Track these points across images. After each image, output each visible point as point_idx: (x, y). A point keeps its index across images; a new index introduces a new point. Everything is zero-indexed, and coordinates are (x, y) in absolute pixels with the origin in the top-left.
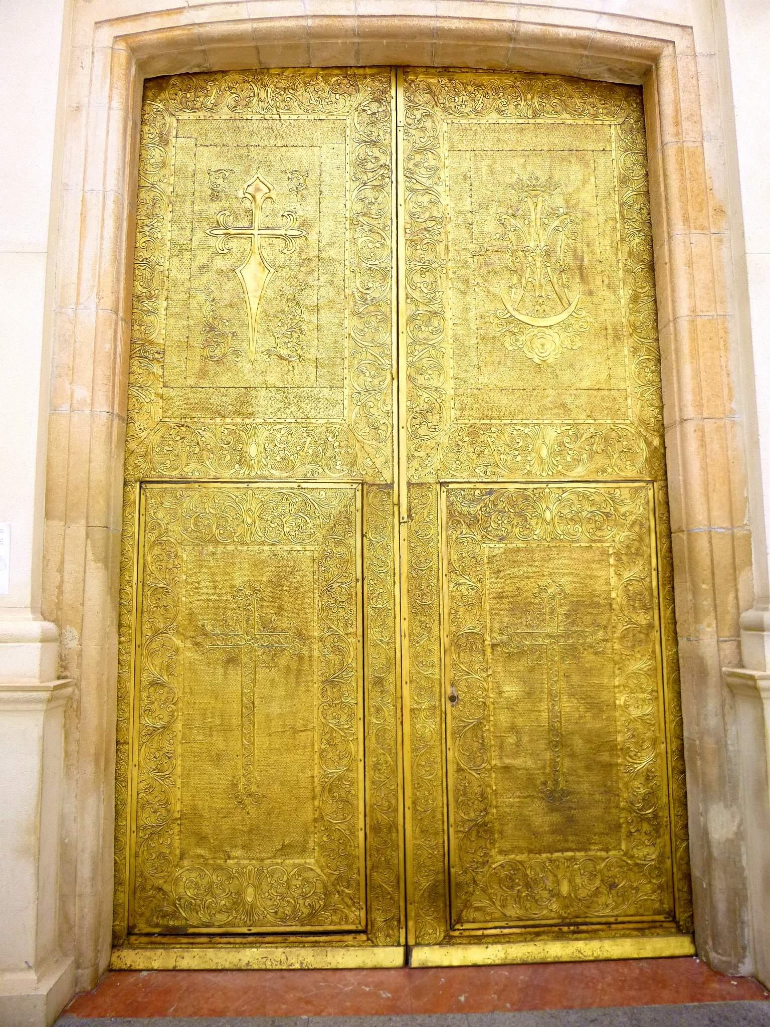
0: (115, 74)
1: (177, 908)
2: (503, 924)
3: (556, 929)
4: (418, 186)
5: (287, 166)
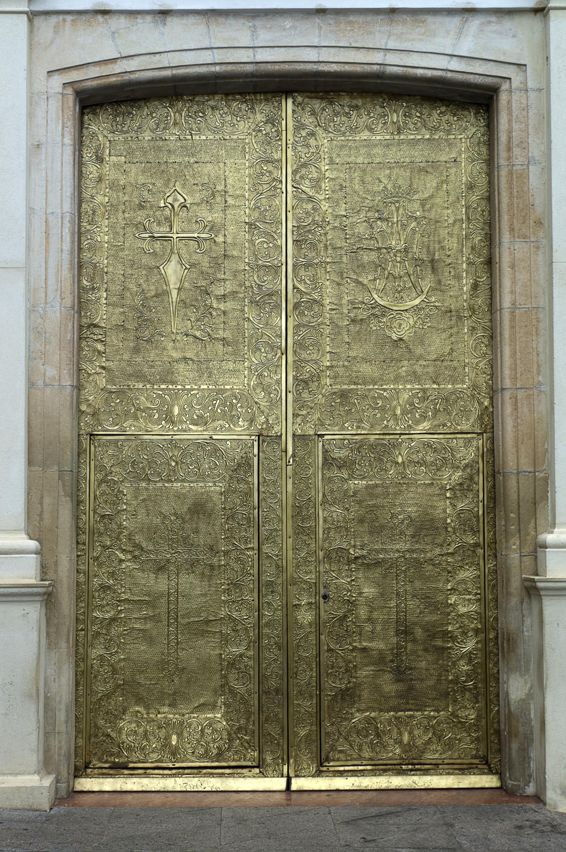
0: (66, 116)
1: (121, 749)
2: (359, 763)
3: (399, 767)
4: (304, 196)
5: (199, 180)
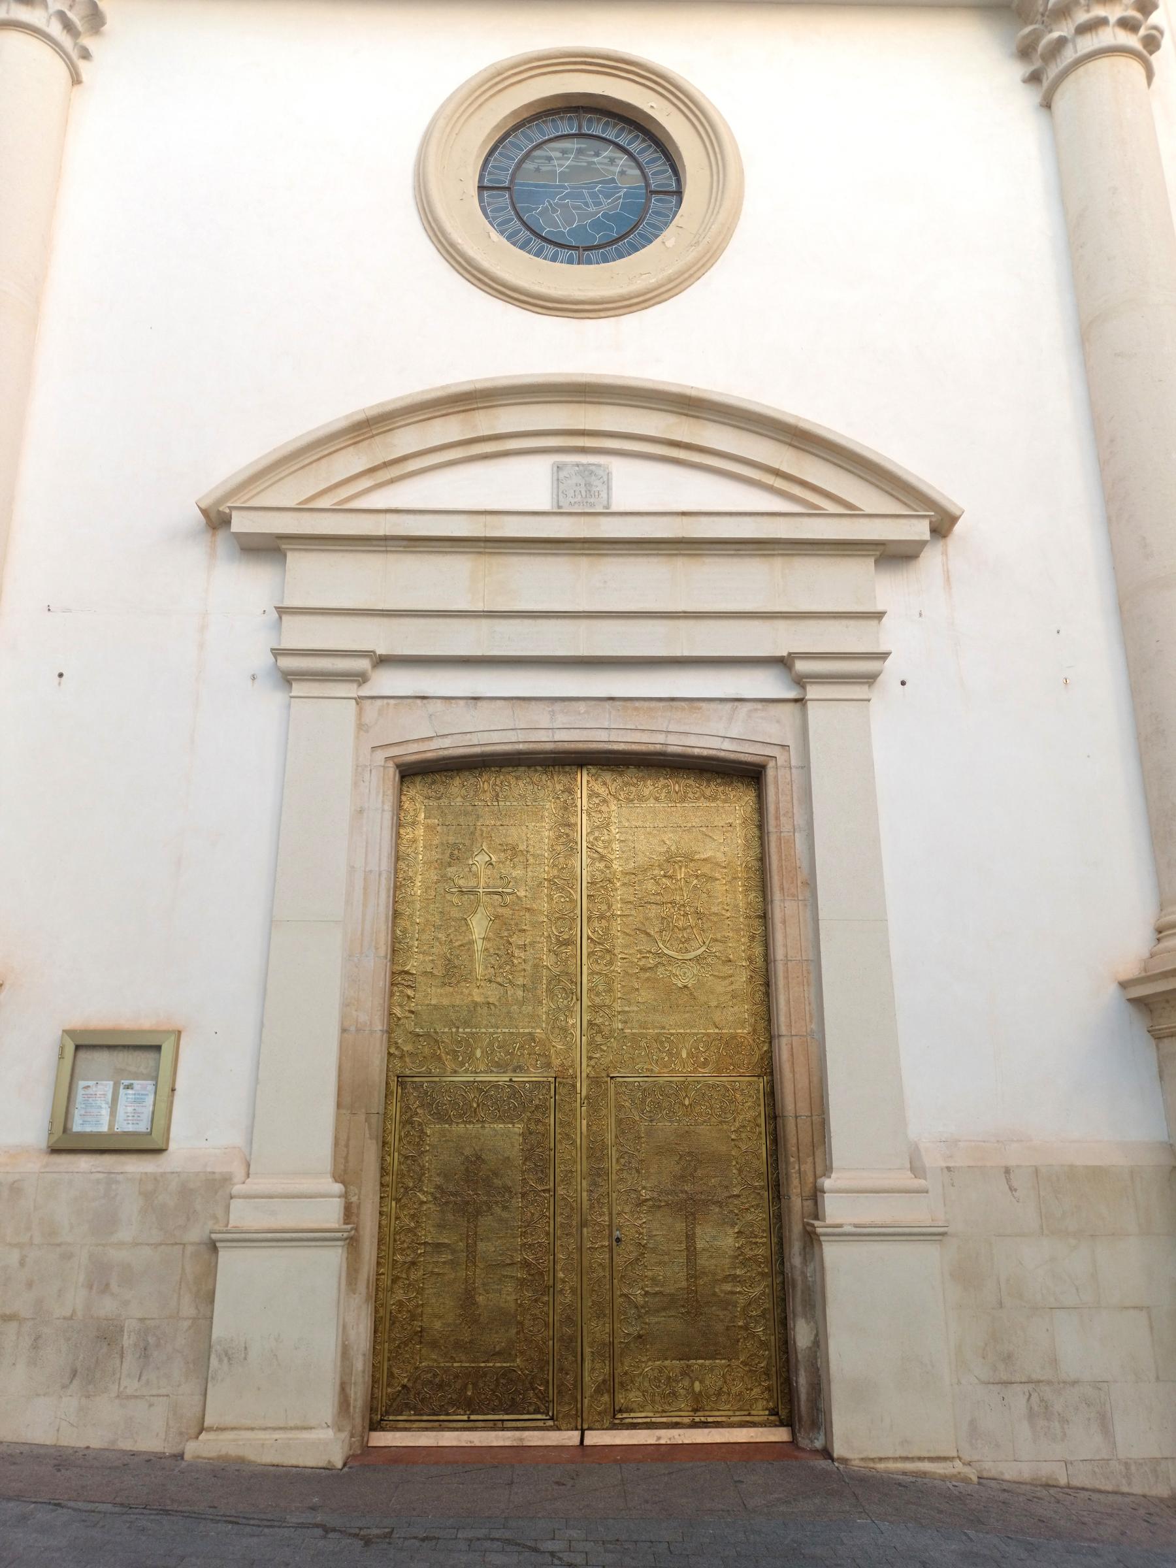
4: (595, 855)
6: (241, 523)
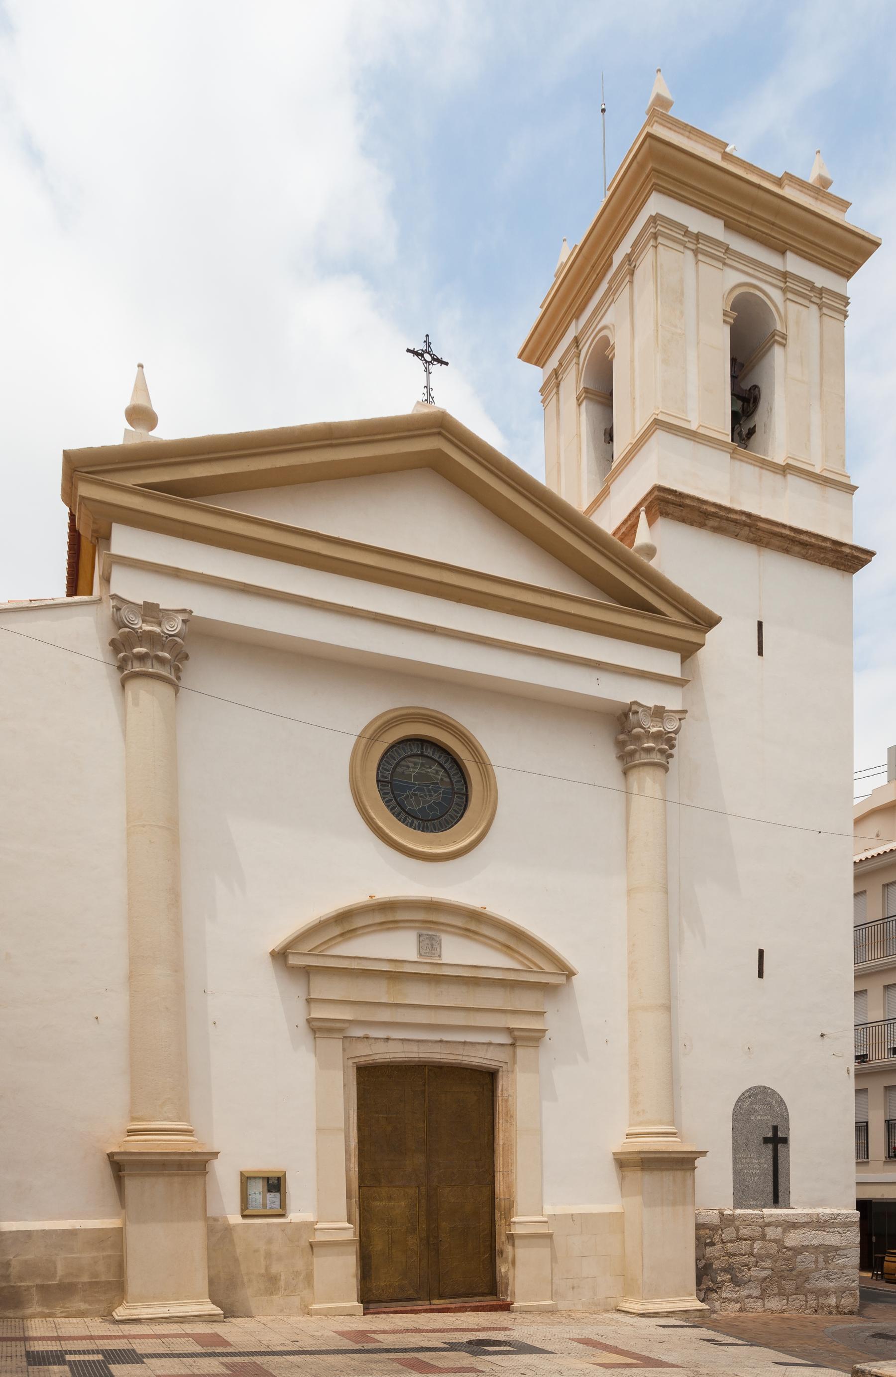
6: (293, 961)
